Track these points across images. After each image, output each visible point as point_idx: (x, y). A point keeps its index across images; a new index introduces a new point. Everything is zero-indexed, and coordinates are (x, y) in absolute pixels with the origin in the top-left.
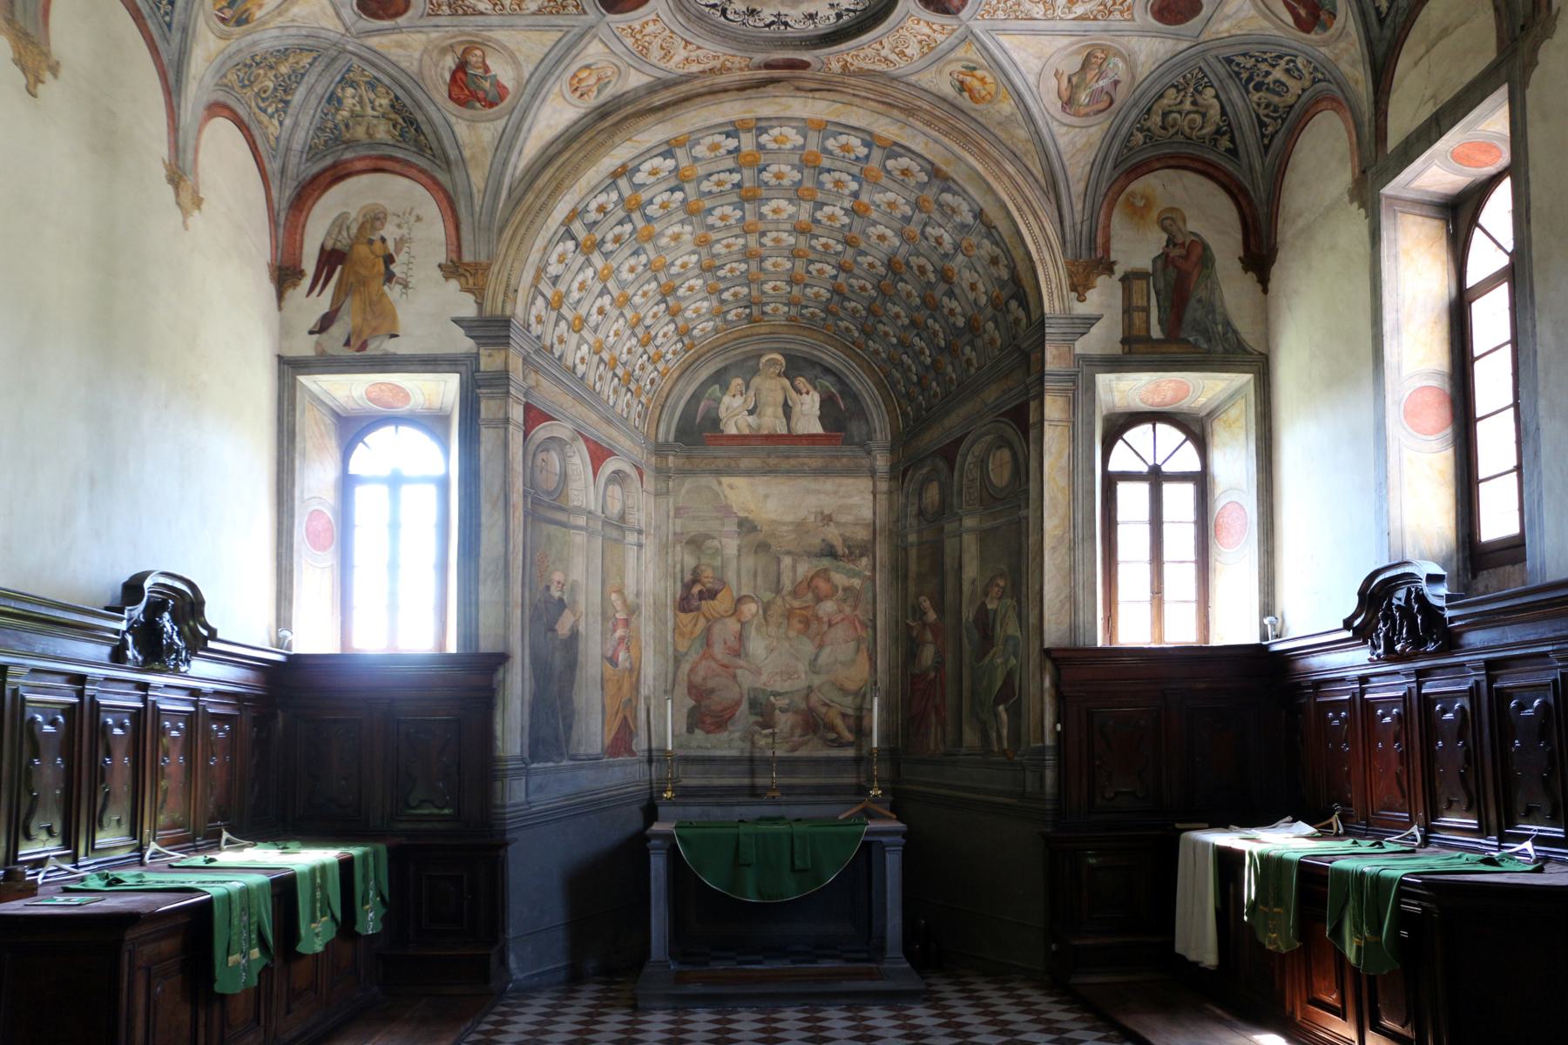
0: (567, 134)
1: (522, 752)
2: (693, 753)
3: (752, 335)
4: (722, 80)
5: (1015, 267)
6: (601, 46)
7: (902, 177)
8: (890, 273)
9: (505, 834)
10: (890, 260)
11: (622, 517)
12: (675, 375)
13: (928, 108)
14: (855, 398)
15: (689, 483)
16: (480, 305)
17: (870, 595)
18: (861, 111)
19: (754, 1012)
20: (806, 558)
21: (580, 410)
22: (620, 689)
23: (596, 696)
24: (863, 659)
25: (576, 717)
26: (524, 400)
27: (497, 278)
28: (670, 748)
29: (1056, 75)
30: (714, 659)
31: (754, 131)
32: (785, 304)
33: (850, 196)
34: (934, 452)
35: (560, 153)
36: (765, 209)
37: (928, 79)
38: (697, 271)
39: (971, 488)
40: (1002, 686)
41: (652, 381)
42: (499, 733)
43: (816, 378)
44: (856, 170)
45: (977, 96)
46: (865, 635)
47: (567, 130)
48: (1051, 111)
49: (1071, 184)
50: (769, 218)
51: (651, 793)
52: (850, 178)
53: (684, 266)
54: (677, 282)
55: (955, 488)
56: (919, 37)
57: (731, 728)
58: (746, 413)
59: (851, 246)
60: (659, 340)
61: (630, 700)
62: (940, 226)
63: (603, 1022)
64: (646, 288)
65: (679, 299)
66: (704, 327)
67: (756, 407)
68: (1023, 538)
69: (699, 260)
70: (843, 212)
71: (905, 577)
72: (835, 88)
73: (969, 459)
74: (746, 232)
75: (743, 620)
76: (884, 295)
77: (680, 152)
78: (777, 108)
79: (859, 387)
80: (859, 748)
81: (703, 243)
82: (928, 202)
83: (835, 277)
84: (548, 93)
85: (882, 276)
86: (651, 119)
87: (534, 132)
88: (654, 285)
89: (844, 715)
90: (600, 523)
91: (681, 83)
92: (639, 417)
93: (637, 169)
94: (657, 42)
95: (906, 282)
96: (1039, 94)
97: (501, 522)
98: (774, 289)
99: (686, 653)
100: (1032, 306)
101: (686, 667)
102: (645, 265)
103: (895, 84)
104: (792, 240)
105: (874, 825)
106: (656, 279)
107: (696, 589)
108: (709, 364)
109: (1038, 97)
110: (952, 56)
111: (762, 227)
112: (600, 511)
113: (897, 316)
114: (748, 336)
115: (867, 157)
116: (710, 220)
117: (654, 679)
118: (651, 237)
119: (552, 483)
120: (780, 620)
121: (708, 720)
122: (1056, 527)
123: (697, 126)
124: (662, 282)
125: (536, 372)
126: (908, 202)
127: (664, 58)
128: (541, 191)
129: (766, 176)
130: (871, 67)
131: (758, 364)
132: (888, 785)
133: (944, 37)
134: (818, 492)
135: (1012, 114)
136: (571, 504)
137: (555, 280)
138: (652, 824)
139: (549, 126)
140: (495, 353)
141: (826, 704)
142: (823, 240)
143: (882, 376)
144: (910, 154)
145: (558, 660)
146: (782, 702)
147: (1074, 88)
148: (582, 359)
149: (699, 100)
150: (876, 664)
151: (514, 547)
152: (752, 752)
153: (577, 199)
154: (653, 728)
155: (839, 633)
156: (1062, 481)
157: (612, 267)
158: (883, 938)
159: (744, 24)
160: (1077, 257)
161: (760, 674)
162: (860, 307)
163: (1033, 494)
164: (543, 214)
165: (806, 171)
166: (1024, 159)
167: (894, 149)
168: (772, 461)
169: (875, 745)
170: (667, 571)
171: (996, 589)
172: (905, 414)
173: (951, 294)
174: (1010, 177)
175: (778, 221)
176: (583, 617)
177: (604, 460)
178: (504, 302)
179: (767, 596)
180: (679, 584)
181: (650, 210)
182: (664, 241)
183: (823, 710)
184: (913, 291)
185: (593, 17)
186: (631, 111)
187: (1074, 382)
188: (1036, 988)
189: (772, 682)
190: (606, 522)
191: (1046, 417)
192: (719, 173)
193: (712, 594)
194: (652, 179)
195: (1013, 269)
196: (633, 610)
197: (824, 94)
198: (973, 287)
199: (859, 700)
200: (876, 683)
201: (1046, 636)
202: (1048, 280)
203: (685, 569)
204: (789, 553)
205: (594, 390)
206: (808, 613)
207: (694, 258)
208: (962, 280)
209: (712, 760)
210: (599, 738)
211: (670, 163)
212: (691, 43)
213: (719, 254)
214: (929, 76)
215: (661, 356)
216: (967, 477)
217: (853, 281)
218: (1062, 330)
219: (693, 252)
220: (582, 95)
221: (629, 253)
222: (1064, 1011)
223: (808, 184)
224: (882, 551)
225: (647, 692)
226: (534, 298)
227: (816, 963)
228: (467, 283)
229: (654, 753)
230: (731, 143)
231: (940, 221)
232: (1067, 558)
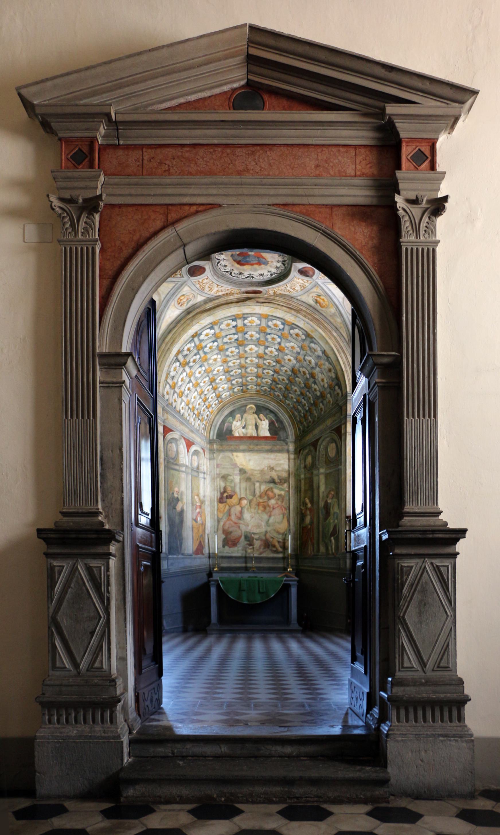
2: (224, 555)
4: (231, 298)
10: (293, 369)
11: (198, 468)
12: (216, 413)
15: (221, 455)
17: (288, 498)
21: (182, 427)
22: (198, 531)
23: (190, 533)
24: (285, 521)
28: (216, 552)
30: (231, 520)
32: (255, 386)
35: (174, 328)
36: (247, 349)
37: (304, 298)
38: (223, 373)
41: (207, 416)
44: (279, 334)
46: (286, 512)
53: (218, 371)
54: (216, 377)
60: (210, 400)
61: (202, 535)
62: (310, 356)
64: (205, 380)
65: (216, 384)
66: (225, 395)
67: (245, 425)
73: (322, 447)
74: (240, 357)
76: (291, 382)
77: (216, 327)
79: (283, 418)
81: (225, 362)
83: (273, 375)
86: (205, 314)
87: (165, 320)
88: (207, 379)
89: (279, 542)
93: (201, 334)
98: (251, 379)
100: (343, 388)
101: (222, 524)
103: (293, 300)
104: (257, 361)
106: (208, 376)
107: (225, 495)
110: (312, 291)
111: (246, 356)
113: (296, 391)
115: (283, 329)
116: (227, 353)
121: (230, 543)
123: (222, 317)
126: (298, 347)
128: (167, 343)
129: (247, 336)
130: (284, 293)
134: (268, 458)
139: (170, 317)
141: (272, 538)
142: (268, 361)
146: (256, 537)
148: (183, 408)
149: (222, 307)
153: (180, 346)
164: (168, 352)
165: (261, 334)
167: (293, 326)
168: (251, 447)
169: (290, 552)
172: (299, 429)
173: (315, 383)
175: (251, 354)
179: (251, 497)
180: (219, 493)
182: (211, 361)
183: (271, 540)
190: (192, 470)
193: (231, 497)
194: (206, 338)
195: (336, 374)
196: (202, 502)
199: (284, 536)
204: (258, 481)
207: (222, 368)
211: (212, 331)
215: (211, 406)
217: (280, 377)
219: (221, 366)
223: (262, 339)
224: (292, 481)
226: (166, 385)
229: (211, 555)
230: (234, 323)
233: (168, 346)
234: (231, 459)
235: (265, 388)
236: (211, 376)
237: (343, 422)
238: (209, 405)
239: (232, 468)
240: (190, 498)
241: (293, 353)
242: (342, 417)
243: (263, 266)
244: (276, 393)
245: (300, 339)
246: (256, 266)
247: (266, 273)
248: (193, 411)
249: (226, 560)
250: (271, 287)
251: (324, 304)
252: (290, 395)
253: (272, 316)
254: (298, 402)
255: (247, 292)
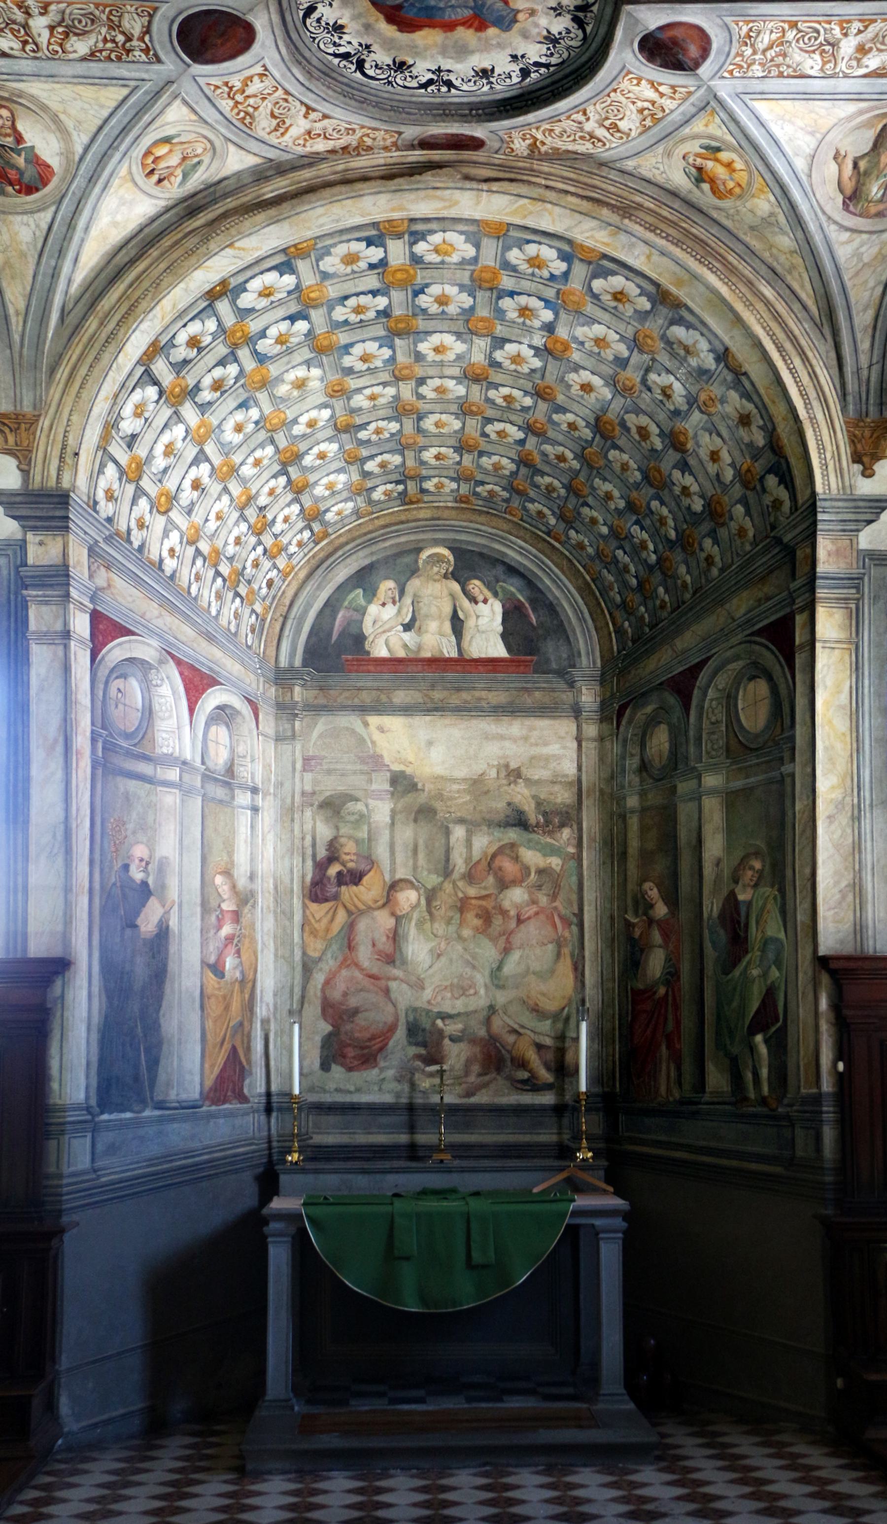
0: (141, 236)
1: (87, 1098)
2: (327, 1098)
3: (408, 521)
4: (361, 163)
5: (774, 429)
6: (185, 110)
7: (614, 304)
8: (598, 436)
9: (60, 1216)
10: (598, 419)
11: (230, 770)
12: (302, 575)
13: (652, 206)
14: (552, 609)
15: (322, 724)
16: (26, 473)
17: (574, 879)
18: (557, 210)
19: (412, 1476)
20: (485, 828)
21: (168, 622)
22: (227, 1008)
23: (195, 1018)
24: (565, 967)
25: (165, 1047)
26: (91, 606)
27: (48, 436)
28: (296, 1091)
29: (835, 158)
30: (357, 965)
31: (406, 236)
32: (452, 479)
33: (541, 329)
34: (661, 684)
35: (132, 262)
36: (424, 347)
38: (330, 432)
39: (713, 733)
40: (758, 1012)
41: (270, 584)
42: (54, 1070)
43: (498, 581)
44: (550, 293)
45: (722, 187)
46: (567, 934)
47: (141, 230)
48: (828, 209)
49: (854, 312)
50: (429, 359)
51: (270, 1155)
52: (543, 303)
53: (311, 424)
54: (303, 447)
55: (691, 733)
56: (640, 104)
57: (382, 1064)
58: (401, 628)
59: (544, 399)
60: (279, 527)
61: (241, 1024)
62: (668, 371)
63: (196, 1496)
64: (258, 454)
65: (305, 469)
67: (413, 619)
68: (788, 803)
69: (332, 416)
70: (532, 352)
71: (624, 855)
72: (519, 177)
73: (711, 693)
74: (398, 379)
75: (399, 913)
76: (591, 467)
77: (302, 266)
78: (438, 205)
79: (557, 593)
80: (561, 1092)
82: (652, 339)
83: (522, 442)
84: (111, 175)
85: (586, 441)
86: (261, 217)
87: (94, 232)
88: (270, 450)
89: (539, 1047)
90: (199, 778)
91: (303, 167)
92: (253, 631)
93: (242, 288)
94: (266, 107)
95: (621, 450)
96: (811, 185)
97: (59, 775)
98: (437, 457)
99: (320, 959)
100: (799, 482)
101: (319, 978)
102: (257, 423)
103: (604, 172)
104: (461, 390)
105: (582, 1202)
106: (272, 441)
107: (333, 870)
108: (348, 561)
109: (808, 189)
110: (687, 131)
111: (419, 372)
112: (198, 760)
113: (608, 496)
114: (402, 522)
115: (566, 275)
116: (347, 361)
117: (275, 995)
118: (265, 384)
119: (132, 721)
120: (450, 914)
121: (351, 1052)
122: (833, 788)
123: (328, 228)
124: (281, 447)
125: (108, 568)
126: (623, 339)
127: (276, 130)
128: (107, 315)
129: (424, 301)
130: (571, 147)
131: (416, 561)
132: (601, 1145)
133: (675, 103)
134: (502, 737)
135: (772, 214)
136: (158, 751)
137: (132, 440)
138: (270, 1200)
139: (115, 224)
140: (48, 540)
141: (514, 1031)
142: (505, 391)
143: (588, 578)
144: (626, 272)
145: (141, 971)
146: (453, 1028)
147: (861, 176)
148: (172, 551)
149: (327, 192)
150: (583, 975)
151: (78, 810)
152: (411, 1097)
153: (158, 328)
154: (272, 1063)
155: (533, 931)
156: (842, 724)
157: (210, 424)
158: (595, 1365)
159: (389, 83)
160: (861, 416)
161: (423, 988)
162: (556, 483)
163: (800, 741)
164: (111, 348)
165: (479, 294)
166: (789, 279)
168: (437, 695)
169: (583, 1088)
170: (293, 844)
171: (750, 873)
172: (619, 631)
173: (684, 467)
174: (767, 303)
175: (442, 364)
176: (176, 908)
177: (204, 690)
178: (59, 469)
179: (433, 880)
180: (309, 863)
181: (263, 346)
182: (283, 390)
183: (511, 1039)
184: (631, 463)
185: (172, 67)
186: (231, 206)
187: (857, 588)
188: (813, 1443)
189: (439, 998)
190: (208, 777)
191: (819, 635)
192: (357, 295)
193: (355, 877)
194: (264, 303)
195: (771, 432)
196: (245, 899)
197: (505, 185)
198: (715, 456)
199: (560, 1025)
200: (583, 1002)
201: (821, 938)
202: (821, 449)
203: (318, 840)
204: (461, 821)
205: (189, 593)
206: (489, 904)
207: (326, 413)
208: (699, 446)
209: (353, 1108)
210: (197, 1079)
211: (289, 280)
212: (314, 110)
213: (360, 409)
214: (654, 160)
215: (282, 549)
216: (708, 718)
217: (548, 448)
218: (840, 517)
219: (325, 406)
220: (160, 181)
221: (235, 404)
222: (857, 1480)
223: (483, 312)
224: (591, 819)
225: (264, 1013)
226: (102, 466)
227: (501, 1400)
228: (6, 441)
229: (274, 1099)
230: (375, 254)
231: (668, 364)
232: (849, 831)
233: (111, 326)
234: (361, 741)
235: (489, 487)
236: (282, 443)
237: (799, 602)
238: (274, 545)
239: (362, 772)
240: (196, 883)
241: (601, 361)
242: (794, 586)
243: (492, 31)
244: (532, 507)
245: (613, 507)
246: (464, 34)
247: (502, 64)
248: (216, 565)
249: (332, 1119)
250: (521, 120)
251: (731, 184)
252: (585, 511)
253: (525, 228)
254: (618, 536)
255: (425, 144)
